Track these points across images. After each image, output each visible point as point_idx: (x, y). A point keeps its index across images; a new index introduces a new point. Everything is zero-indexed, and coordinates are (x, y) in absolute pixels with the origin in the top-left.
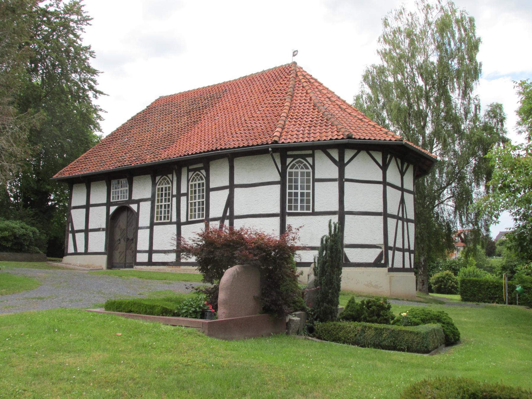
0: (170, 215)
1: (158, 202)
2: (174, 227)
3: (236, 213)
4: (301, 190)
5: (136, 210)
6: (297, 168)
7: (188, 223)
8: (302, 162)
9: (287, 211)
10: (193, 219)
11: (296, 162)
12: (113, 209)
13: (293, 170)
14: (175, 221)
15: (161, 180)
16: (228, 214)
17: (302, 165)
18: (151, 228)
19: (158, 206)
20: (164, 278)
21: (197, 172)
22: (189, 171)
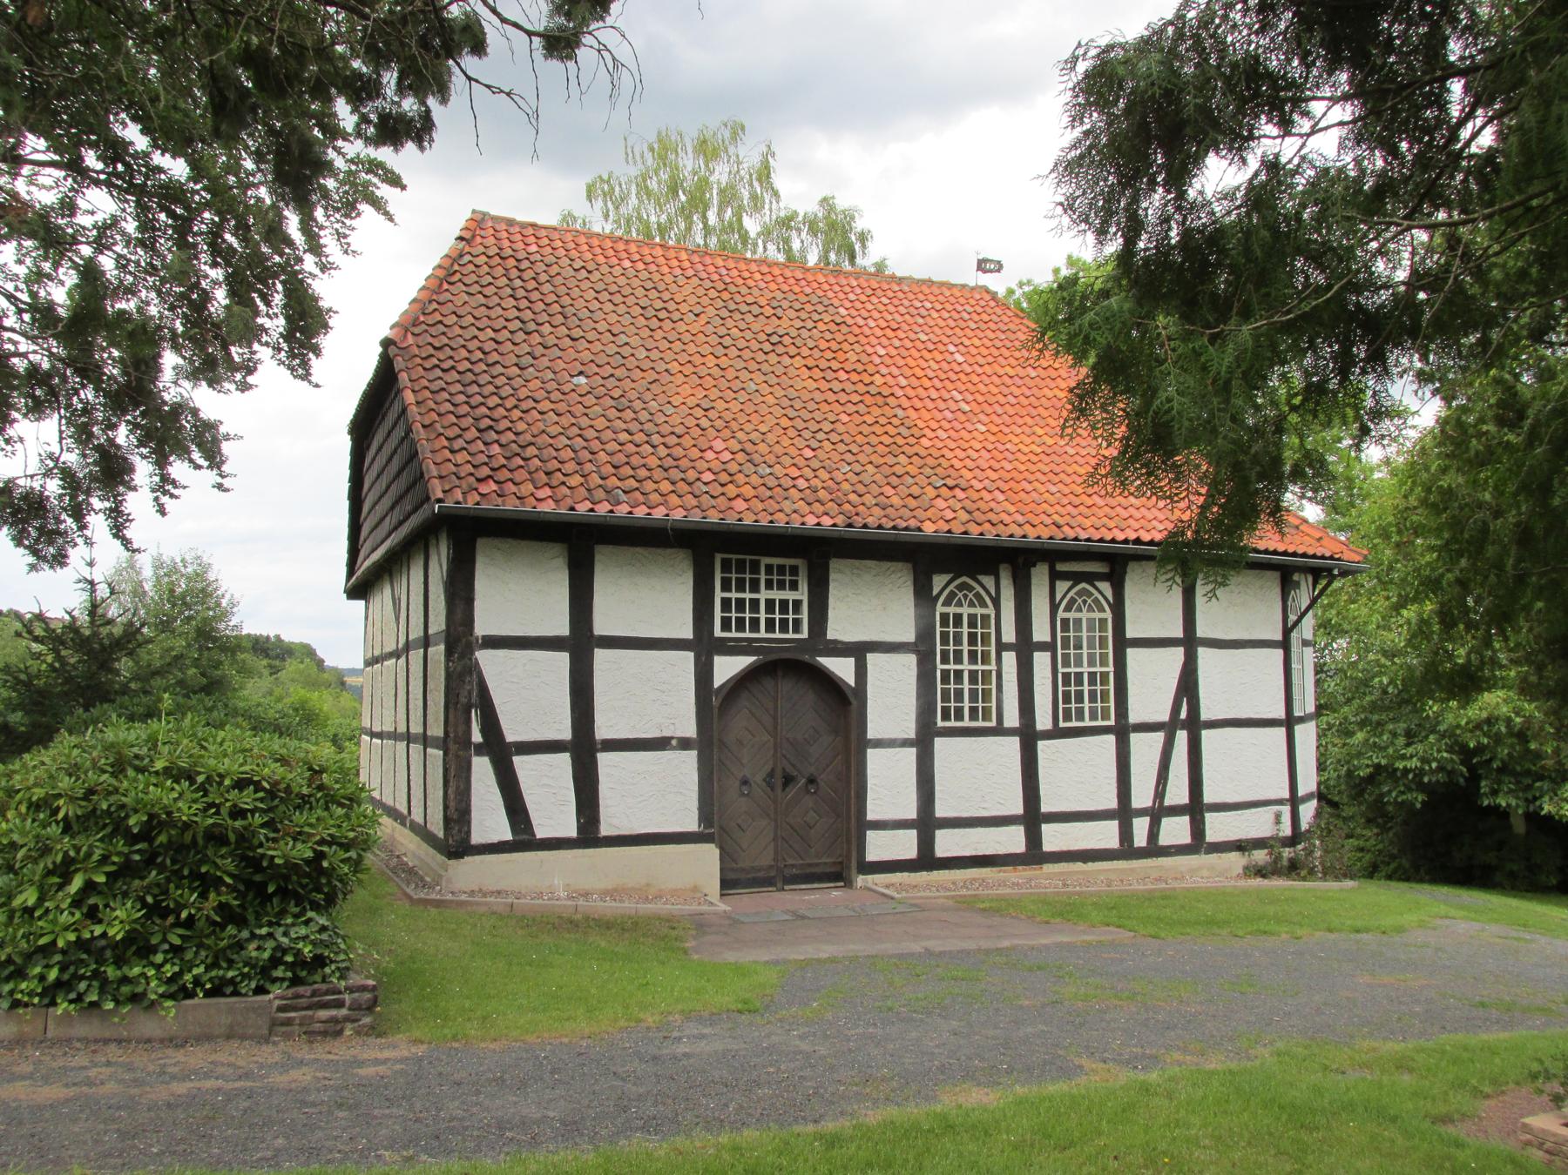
0: (994, 704)
1: (945, 660)
2: (1014, 743)
3: (1205, 715)
4: (970, 663)
5: (850, 679)
6: (960, 604)
7: (1057, 733)
8: (971, 589)
9: (940, 723)
10: (1074, 724)
11: (956, 587)
12: (726, 668)
13: (1071, 615)
14: (1017, 724)
15: (951, 587)
16: (1183, 715)
17: (971, 595)
18: (924, 742)
19: (945, 674)
20: (999, 909)
21: (1084, 585)
22: (1055, 576)
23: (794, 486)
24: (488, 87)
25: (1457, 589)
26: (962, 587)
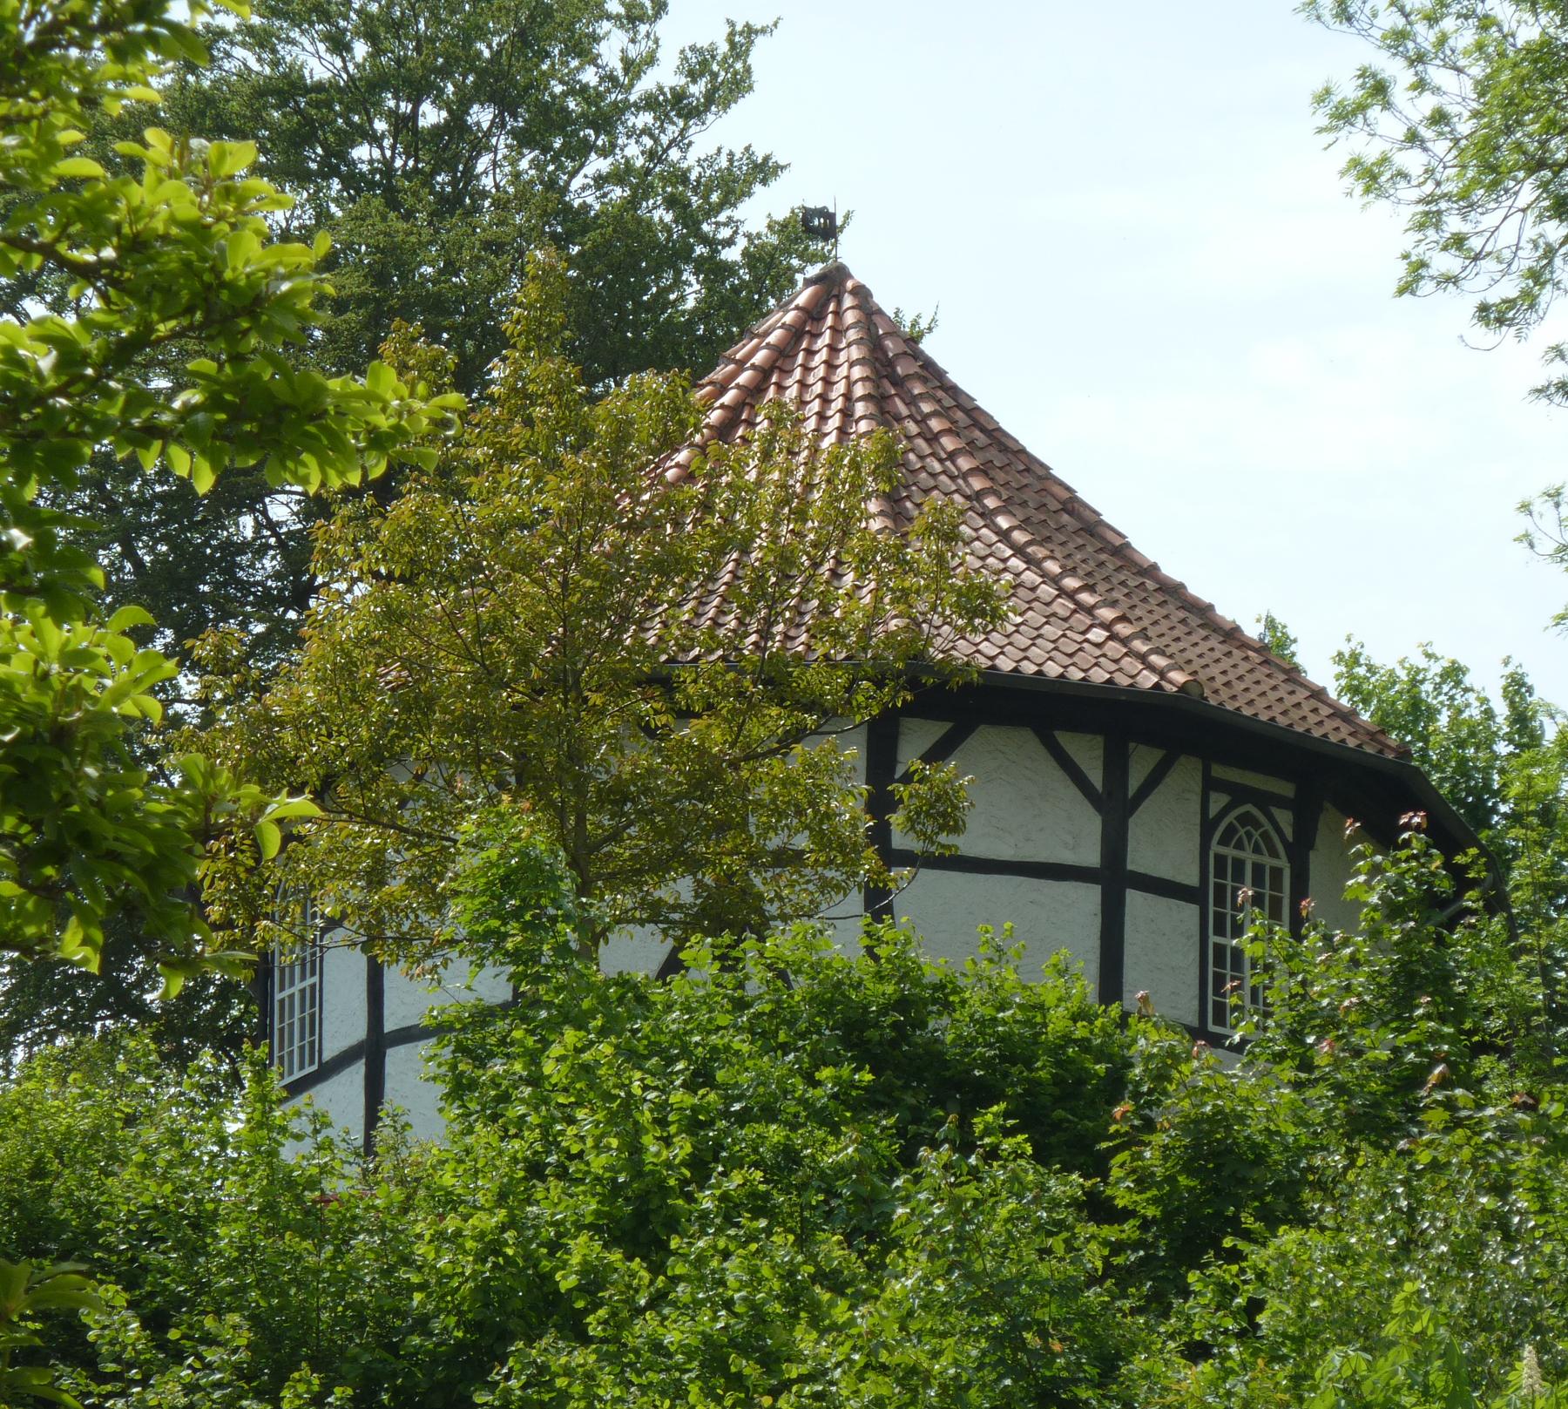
6: (1239, 846)
23: (923, 468)
24: (1506, 218)
25: (840, 571)
26: (1245, 819)
